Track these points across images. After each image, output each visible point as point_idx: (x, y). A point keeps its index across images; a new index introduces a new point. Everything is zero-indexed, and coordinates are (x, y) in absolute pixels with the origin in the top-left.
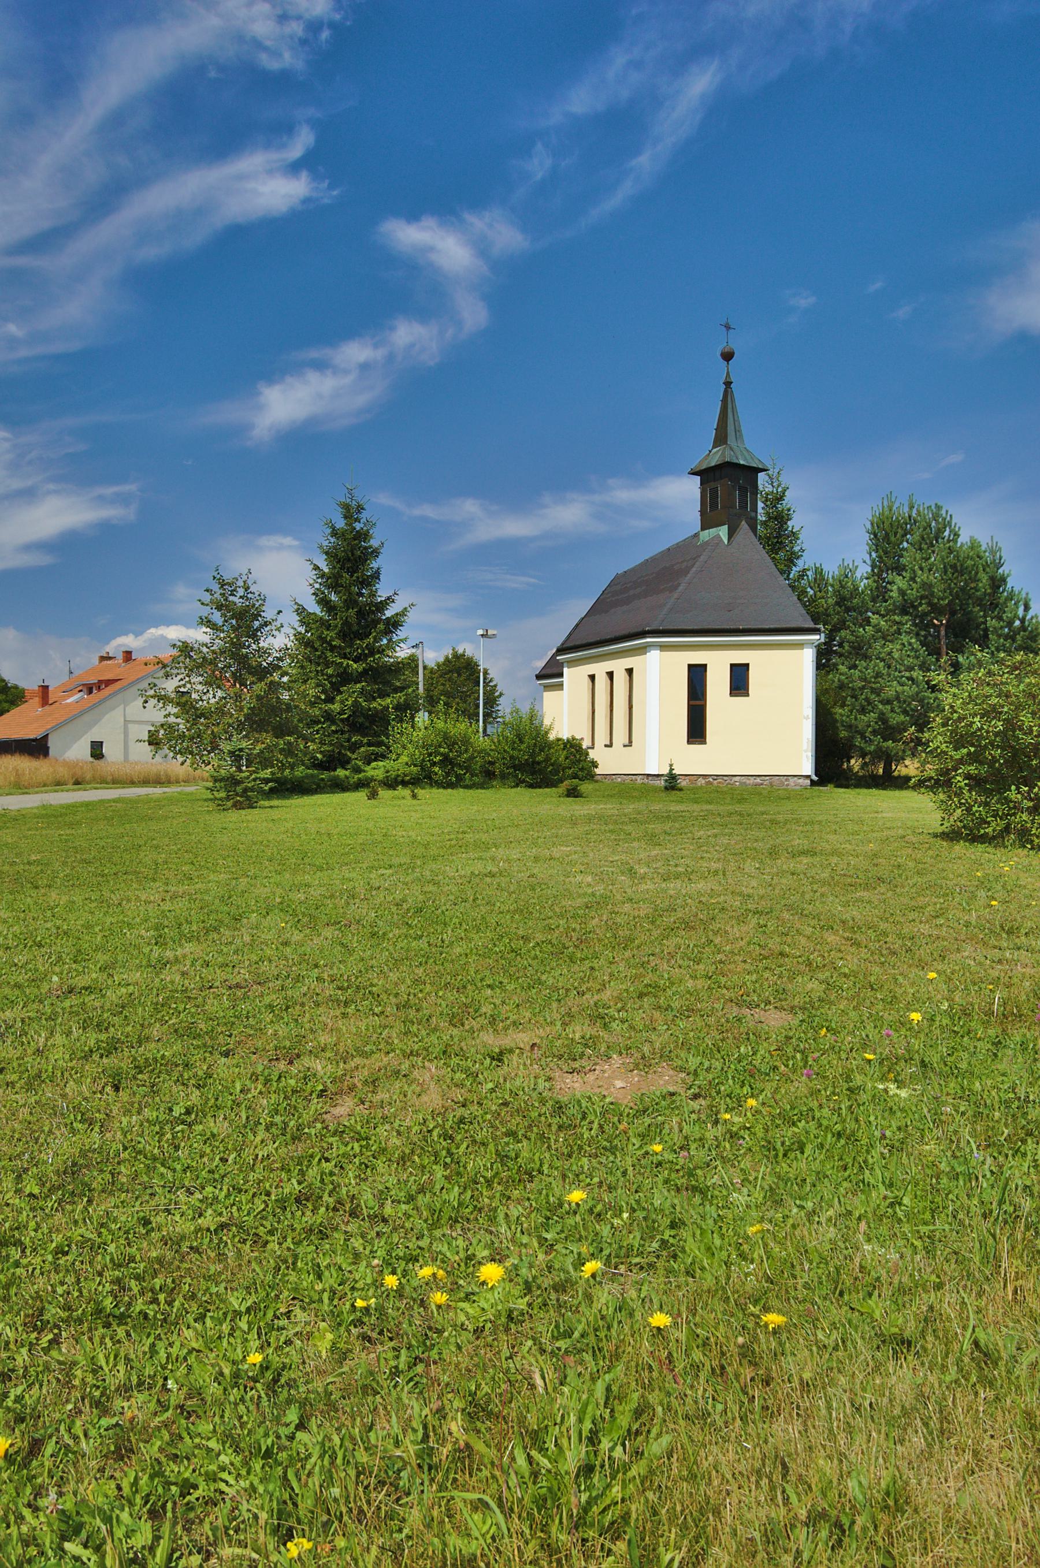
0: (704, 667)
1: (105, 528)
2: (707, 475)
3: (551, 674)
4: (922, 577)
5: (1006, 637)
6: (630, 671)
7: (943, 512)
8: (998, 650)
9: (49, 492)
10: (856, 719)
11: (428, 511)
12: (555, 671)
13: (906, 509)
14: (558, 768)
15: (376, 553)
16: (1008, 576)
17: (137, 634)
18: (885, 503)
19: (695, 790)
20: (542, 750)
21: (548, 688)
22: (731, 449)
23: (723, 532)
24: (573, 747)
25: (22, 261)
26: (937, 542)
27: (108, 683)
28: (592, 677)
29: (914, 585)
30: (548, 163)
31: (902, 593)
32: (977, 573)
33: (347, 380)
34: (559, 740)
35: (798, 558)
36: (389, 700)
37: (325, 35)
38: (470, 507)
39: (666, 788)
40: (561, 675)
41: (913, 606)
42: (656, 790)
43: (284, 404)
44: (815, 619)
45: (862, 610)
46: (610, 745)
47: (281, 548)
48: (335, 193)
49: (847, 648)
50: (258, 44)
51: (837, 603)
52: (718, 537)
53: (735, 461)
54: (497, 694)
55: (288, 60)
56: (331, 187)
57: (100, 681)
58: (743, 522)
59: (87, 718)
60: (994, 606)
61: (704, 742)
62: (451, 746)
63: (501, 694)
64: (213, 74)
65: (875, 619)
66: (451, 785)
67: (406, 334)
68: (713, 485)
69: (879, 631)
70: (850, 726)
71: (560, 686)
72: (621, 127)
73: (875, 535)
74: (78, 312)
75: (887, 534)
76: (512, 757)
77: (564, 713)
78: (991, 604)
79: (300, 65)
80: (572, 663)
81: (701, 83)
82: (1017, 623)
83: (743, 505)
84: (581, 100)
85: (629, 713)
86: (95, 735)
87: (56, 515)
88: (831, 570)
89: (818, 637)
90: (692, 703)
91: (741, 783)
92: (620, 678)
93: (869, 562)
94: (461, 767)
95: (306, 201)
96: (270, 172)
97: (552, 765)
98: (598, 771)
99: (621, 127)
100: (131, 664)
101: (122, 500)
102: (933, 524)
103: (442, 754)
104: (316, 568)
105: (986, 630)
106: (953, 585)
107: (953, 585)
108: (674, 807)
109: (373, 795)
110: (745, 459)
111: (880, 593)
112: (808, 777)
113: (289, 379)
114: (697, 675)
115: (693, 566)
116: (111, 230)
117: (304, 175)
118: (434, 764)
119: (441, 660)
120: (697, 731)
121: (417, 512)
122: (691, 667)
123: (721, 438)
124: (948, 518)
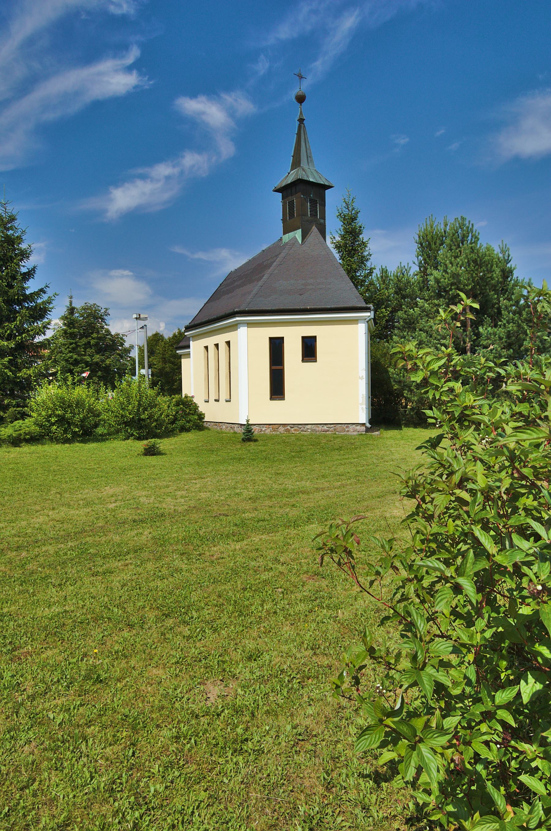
0: (314, 338)
2: (286, 190)
4: (451, 269)
5: (514, 313)
6: (228, 343)
7: (467, 222)
8: (508, 322)
10: (404, 377)
11: (200, 255)
13: (442, 227)
16: (514, 269)
18: (428, 223)
19: (270, 438)
22: (304, 170)
23: (298, 234)
26: (463, 244)
28: (206, 348)
29: (446, 276)
30: (267, 65)
31: (437, 281)
32: (492, 266)
33: (159, 185)
35: (367, 260)
40: (188, 347)
41: (445, 291)
43: (124, 198)
44: (367, 301)
45: (413, 297)
47: (122, 276)
48: (151, 83)
49: (401, 323)
51: (396, 293)
52: (295, 238)
53: (305, 178)
56: (149, 80)
58: (314, 227)
60: (504, 291)
61: (283, 398)
64: (83, 17)
67: (190, 159)
68: (290, 198)
69: (424, 311)
70: (400, 382)
72: (307, 45)
73: (421, 244)
75: (429, 244)
78: (503, 289)
79: (132, 12)
82: (522, 302)
83: (314, 213)
84: (285, 32)
89: (368, 314)
90: (274, 367)
92: (223, 347)
93: (417, 263)
95: (136, 87)
96: (116, 71)
97: (156, 420)
99: (307, 45)
102: (460, 231)
103: (58, 416)
105: (499, 309)
106: (474, 275)
107: (474, 275)
110: (314, 178)
111: (424, 285)
112: (363, 424)
113: (126, 185)
114: (276, 346)
115: (274, 261)
117: (135, 72)
119: (171, 336)
120: (277, 389)
122: (272, 339)
123: (296, 163)
124: (471, 226)
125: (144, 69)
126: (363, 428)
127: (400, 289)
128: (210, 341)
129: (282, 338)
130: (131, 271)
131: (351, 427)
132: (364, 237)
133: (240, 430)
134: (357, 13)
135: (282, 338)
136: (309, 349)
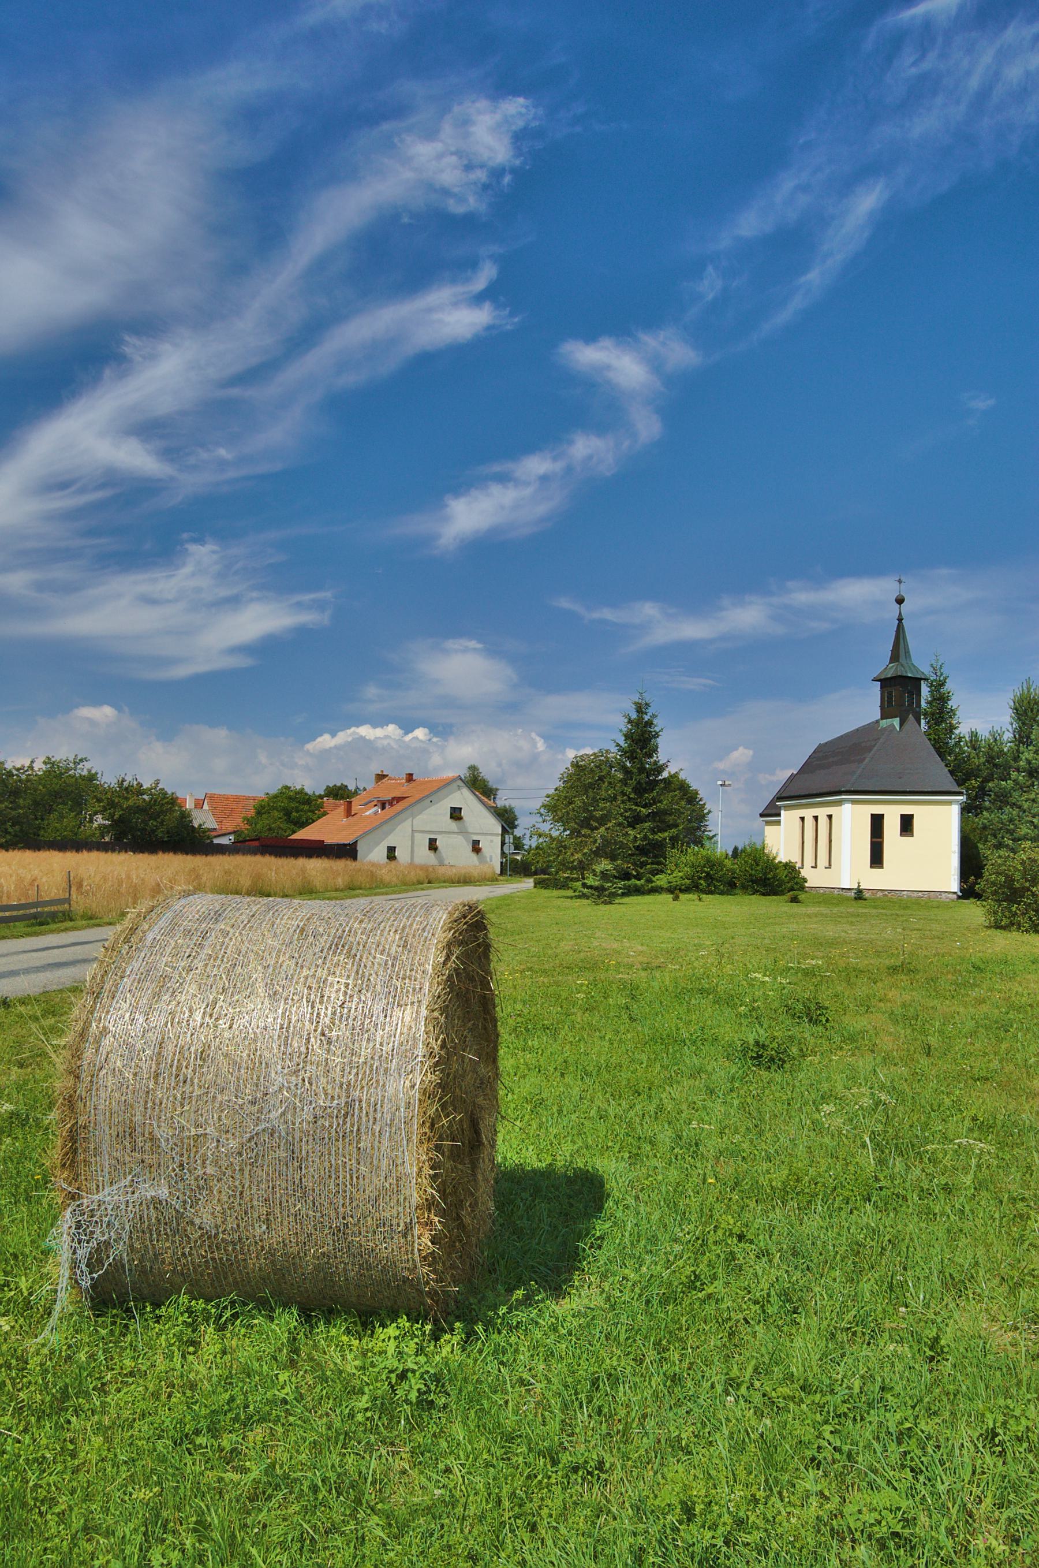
1: (302, 634)
2: (886, 683)
3: (771, 813)
6: (830, 817)
9: (252, 600)
11: (608, 614)
12: (773, 812)
14: (781, 883)
15: (657, 735)
17: (333, 735)
20: (771, 871)
21: (768, 823)
23: (896, 722)
24: (789, 867)
25: (235, 392)
27: (399, 799)
28: (802, 819)
31: (1029, 762)
33: (528, 491)
34: (780, 862)
36: (666, 834)
37: (507, 179)
38: (649, 610)
39: (856, 898)
40: (779, 815)
42: (848, 899)
43: (469, 515)
46: (815, 867)
47: (466, 650)
48: (516, 320)
50: (445, 192)
51: (987, 761)
54: (706, 811)
55: (473, 203)
56: (512, 315)
57: (393, 798)
59: (385, 828)
61: (882, 867)
62: (712, 867)
63: (710, 812)
64: (406, 220)
65: (1014, 775)
66: (711, 893)
67: (583, 447)
71: (778, 823)
72: (792, 244)
74: (280, 435)
76: (751, 875)
77: (782, 841)
79: (483, 208)
80: (788, 808)
81: (868, 201)
84: (750, 224)
85: (832, 846)
86: (390, 841)
87: (259, 620)
88: (984, 733)
90: (875, 840)
91: (908, 896)
92: (823, 822)
94: (718, 881)
95: (489, 328)
96: (455, 304)
98: (806, 885)
99: (792, 244)
100: (413, 784)
101: (320, 606)
104: (618, 745)
108: (861, 910)
109: (676, 898)
114: (877, 821)
116: (316, 360)
118: (700, 878)
120: (877, 859)
121: (596, 615)
125: (502, 299)
126: (955, 896)
127: (993, 758)
128: (808, 813)
129: (883, 815)
130: (479, 642)
131: (944, 895)
132: (952, 704)
133: (852, 894)
134: (879, 187)
135: (883, 815)
136: (907, 824)
